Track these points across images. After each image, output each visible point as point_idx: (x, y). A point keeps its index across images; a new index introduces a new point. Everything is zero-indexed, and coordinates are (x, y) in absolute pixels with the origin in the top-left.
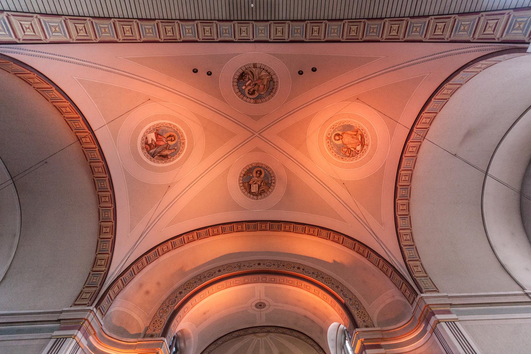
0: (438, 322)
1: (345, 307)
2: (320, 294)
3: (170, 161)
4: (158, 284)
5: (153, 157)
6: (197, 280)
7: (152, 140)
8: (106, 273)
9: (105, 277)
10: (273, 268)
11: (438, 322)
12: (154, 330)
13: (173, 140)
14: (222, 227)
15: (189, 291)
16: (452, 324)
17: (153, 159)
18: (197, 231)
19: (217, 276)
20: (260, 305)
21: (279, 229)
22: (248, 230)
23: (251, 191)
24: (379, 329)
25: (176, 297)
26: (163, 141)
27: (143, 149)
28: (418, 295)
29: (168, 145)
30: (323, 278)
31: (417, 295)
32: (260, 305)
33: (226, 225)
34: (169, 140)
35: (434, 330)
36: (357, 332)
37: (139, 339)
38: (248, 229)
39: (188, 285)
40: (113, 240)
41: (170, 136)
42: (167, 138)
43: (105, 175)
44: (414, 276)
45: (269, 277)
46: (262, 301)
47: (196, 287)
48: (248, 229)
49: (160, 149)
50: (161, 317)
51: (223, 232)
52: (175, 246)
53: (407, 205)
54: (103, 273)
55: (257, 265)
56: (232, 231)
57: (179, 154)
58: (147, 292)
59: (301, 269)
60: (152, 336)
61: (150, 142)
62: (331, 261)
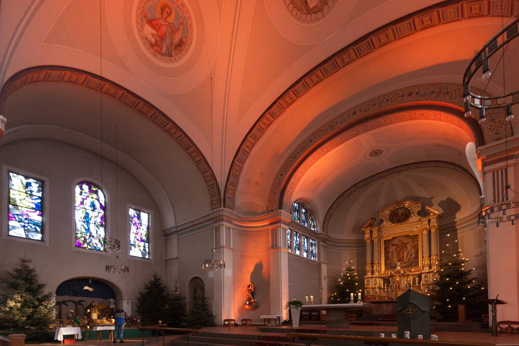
2: (443, 118)
3: (190, 45)
4: (262, 174)
5: (171, 56)
6: (292, 159)
7: (153, 35)
8: (217, 184)
9: (218, 187)
10: (373, 111)
12: (272, 207)
13: (169, 13)
14: (293, 91)
15: (288, 171)
17: (172, 59)
18: (268, 112)
19: (310, 147)
20: (376, 153)
21: (372, 48)
22: (328, 75)
23: (309, 7)
25: (280, 179)
26: (161, 25)
27: (154, 55)
29: (172, 26)
32: (376, 153)
33: (296, 85)
34: (167, 17)
36: (479, 150)
37: (265, 215)
38: (327, 74)
39: (286, 166)
40: (203, 159)
41: (163, 10)
42: (162, 15)
43: (154, 111)
45: (369, 124)
46: (375, 149)
47: (293, 165)
48: (327, 74)
49: (169, 39)
50: (274, 198)
51: (298, 95)
52: (256, 138)
53: (271, 122)
54: (215, 185)
55: (351, 115)
56: (307, 87)
57: (190, 25)
58: (257, 184)
60: (272, 211)
61: (153, 40)
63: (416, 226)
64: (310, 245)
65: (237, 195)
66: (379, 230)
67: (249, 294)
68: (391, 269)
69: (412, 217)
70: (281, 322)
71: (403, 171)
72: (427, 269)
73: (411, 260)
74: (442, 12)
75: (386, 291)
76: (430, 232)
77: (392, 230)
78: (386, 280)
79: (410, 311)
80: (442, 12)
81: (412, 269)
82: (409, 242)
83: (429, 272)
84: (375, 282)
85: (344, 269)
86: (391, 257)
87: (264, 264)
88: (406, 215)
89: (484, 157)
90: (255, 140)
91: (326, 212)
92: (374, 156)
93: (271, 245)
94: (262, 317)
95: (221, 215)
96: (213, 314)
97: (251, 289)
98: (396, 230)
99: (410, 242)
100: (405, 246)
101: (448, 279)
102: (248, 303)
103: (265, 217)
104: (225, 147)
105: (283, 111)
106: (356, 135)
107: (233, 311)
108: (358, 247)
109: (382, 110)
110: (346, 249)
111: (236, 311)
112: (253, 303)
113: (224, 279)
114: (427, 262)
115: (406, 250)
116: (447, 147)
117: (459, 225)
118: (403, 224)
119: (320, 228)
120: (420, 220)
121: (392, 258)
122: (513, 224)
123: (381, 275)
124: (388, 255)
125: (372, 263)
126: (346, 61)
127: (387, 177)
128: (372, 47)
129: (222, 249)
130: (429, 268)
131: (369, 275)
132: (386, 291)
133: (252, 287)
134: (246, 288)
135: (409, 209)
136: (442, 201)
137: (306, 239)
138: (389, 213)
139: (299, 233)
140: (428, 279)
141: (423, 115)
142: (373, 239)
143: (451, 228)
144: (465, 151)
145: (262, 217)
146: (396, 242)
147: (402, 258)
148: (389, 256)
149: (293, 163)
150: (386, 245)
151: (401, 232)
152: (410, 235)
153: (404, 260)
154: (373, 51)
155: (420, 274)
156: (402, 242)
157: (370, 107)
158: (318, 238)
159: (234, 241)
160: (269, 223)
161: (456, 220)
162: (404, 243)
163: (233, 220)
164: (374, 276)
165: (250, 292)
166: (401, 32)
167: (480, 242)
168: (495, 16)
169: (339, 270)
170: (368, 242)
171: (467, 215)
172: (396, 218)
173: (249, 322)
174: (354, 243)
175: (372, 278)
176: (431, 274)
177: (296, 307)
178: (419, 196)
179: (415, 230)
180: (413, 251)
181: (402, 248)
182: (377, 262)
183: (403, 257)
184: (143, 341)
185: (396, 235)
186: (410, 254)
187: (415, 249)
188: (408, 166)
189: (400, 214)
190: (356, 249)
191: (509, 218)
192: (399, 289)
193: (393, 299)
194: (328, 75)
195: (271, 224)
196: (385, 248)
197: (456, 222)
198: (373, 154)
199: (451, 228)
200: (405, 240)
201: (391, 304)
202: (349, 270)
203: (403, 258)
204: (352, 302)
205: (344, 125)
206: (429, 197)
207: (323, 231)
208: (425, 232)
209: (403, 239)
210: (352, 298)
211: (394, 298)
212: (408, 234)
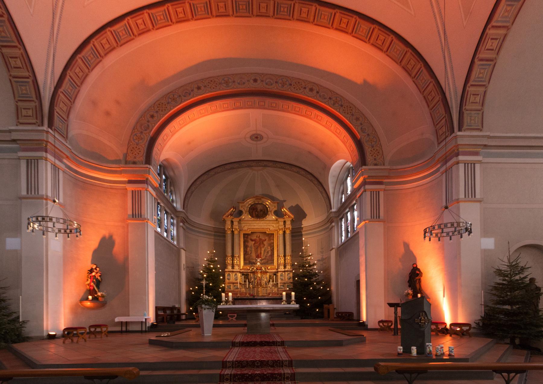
0: (458, 163)
1: (359, 144)
2: (332, 128)
10: (274, 88)
16: (471, 167)
20: (256, 137)
24: (389, 167)
32: (257, 138)
37: (122, 165)
45: (269, 101)
46: (258, 132)
55: (252, 81)
58: (108, 114)
59: (315, 92)
60: (134, 163)
63: (273, 225)
64: (169, 224)
65: (72, 116)
66: (239, 222)
67: (92, 284)
68: (249, 264)
69: (269, 215)
70: (147, 325)
71: (269, 166)
72: (282, 268)
73: (267, 258)
75: (247, 287)
76: (284, 233)
77: (252, 225)
78: (246, 275)
79: (423, 320)
81: (269, 266)
82: (266, 240)
83: (285, 271)
84: (236, 277)
85: (205, 259)
86: (250, 252)
87: (118, 240)
88: (264, 212)
89: (366, 176)
90: (117, 43)
91: (189, 187)
92: (253, 140)
93: (131, 214)
94: (117, 320)
95: (43, 140)
96: (18, 317)
97: (95, 276)
98: (255, 225)
99: (267, 239)
101: (306, 280)
102: (90, 297)
103: (122, 169)
104: (60, 21)
105: (208, 16)
106: (250, 108)
107: (62, 310)
108: (215, 235)
110: (203, 236)
111: (67, 311)
112: (100, 298)
113: (47, 255)
114: (282, 261)
115: (263, 247)
116: (317, 157)
118: (262, 221)
119: (181, 204)
120: (277, 220)
121: (251, 254)
122: (68, 237)
123: (240, 270)
124: (247, 249)
125: (233, 256)
127: (254, 168)
129: (44, 201)
130: (284, 267)
131: (230, 268)
132: (247, 287)
133: (97, 273)
134: (85, 273)
135: (267, 206)
136: (292, 206)
137: (166, 215)
138: (249, 207)
139: (160, 205)
140: (283, 278)
141: (318, 116)
142: (233, 230)
143: (297, 232)
144: (332, 166)
145: (114, 167)
146: (254, 237)
147: (260, 255)
148: (248, 251)
149: (172, 107)
150: (245, 238)
152: (267, 233)
153: (262, 257)
155: (275, 272)
156: (260, 238)
157: (272, 82)
158: (177, 217)
159: (64, 193)
160: (127, 180)
161: (302, 226)
162: (261, 239)
163: (65, 156)
164: (234, 270)
165: (95, 280)
167: (322, 249)
169: (196, 259)
170: (229, 232)
171: (312, 224)
172: (255, 213)
173: (104, 329)
174: (211, 231)
175: (233, 272)
176: (286, 273)
177: (210, 307)
178: (274, 196)
179: (272, 228)
181: (260, 244)
182: (237, 256)
183: (261, 253)
186: (267, 251)
187: (271, 247)
188: (274, 163)
190: (213, 237)
191: (448, 234)
192: (260, 286)
193: (254, 296)
194: (238, 14)
195: (130, 182)
196: (244, 242)
197: (302, 228)
198: (254, 138)
199: (297, 232)
200: (262, 237)
202: (211, 261)
203: (261, 255)
205: (241, 88)
206: (282, 200)
207: (184, 209)
208: (281, 232)
210: (284, 298)
211: (255, 295)
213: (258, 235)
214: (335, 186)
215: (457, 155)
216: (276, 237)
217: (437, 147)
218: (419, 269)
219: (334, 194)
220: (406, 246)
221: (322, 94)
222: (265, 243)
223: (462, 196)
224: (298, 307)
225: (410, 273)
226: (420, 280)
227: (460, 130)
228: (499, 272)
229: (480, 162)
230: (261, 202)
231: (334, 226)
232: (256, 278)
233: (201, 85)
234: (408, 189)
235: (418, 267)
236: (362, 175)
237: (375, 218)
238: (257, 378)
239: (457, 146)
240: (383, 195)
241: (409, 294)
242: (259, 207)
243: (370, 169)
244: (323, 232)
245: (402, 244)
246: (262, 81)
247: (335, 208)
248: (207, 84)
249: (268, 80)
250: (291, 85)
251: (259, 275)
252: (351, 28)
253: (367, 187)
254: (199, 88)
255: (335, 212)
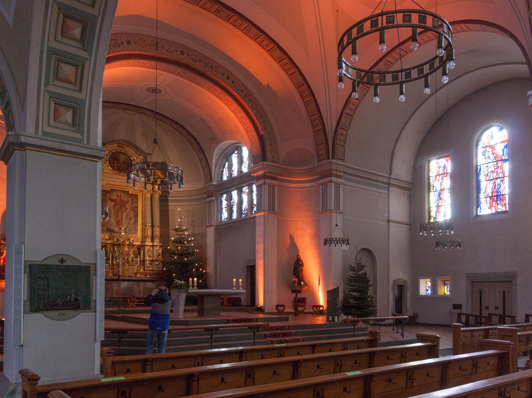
0: (331, 182)
1: (261, 138)
10: (199, 66)
11: (331, 182)
16: (337, 185)
20: (155, 90)
21: (228, 19)
24: (282, 166)
28: (329, 159)
30: (250, 101)
31: (328, 158)
35: (324, 185)
44: (336, 142)
45: (189, 73)
59: (231, 81)
62: (264, 82)
68: (107, 232)
72: (148, 243)
74: (275, 49)
80: (275, 49)
82: (128, 202)
89: (266, 171)
98: (116, 180)
100: (124, 206)
109: (206, 72)
117: (172, 197)
126: (206, 7)
128: (227, 19)
151: (121, 185)
152: (130, 192)
153: (123, 224)
154: (225, 21)
166: (346, 125)
168: (291, 79)
180: (132, 215)
181: (121, 207)
183: (122, 219)
184: (254, 342)
185: (115, 187)
189: (121, 160)
201: (143, 282)
204: (235, 288)
205: (169, 56)
209: (123, 195)
212: (128, 190)
213: (119, 193)
214: (219, 158)
215: (331, 175)
216: (141, 200)
217: (317, 163)
218: (301, 260)
219: (216, 165)
220: (292, 238)
221: (236, 85)
222: (128, 206)
223: (333, 208)
224: (245, 292)
225: (295, 263)
226: (302, 269)
227: (333, 158)
228: (352, 269)
229: (343, 184)
230: (124, 152)
231: (214, 201)
232: (122, 253)
233: (131, 40)
234: (294, 188)
235: (301, 258)
236: (264, 168)
237: (271, 210)
238: (281, 335)
239: (331, 169)
240: (277, 189)
241: (295, 281)
242: (122, 158)
243: (269, 165)
244: (194, 203)
245: (289, 236)
246: (188, 55)
247: (215, 180)
248: (137, 41)
249: (193, 56)
250: (212, 67)
251: (126, 249)
252: (269, 48)
253: (267, 181)
254: (129, 42)
255: (216, 186)
